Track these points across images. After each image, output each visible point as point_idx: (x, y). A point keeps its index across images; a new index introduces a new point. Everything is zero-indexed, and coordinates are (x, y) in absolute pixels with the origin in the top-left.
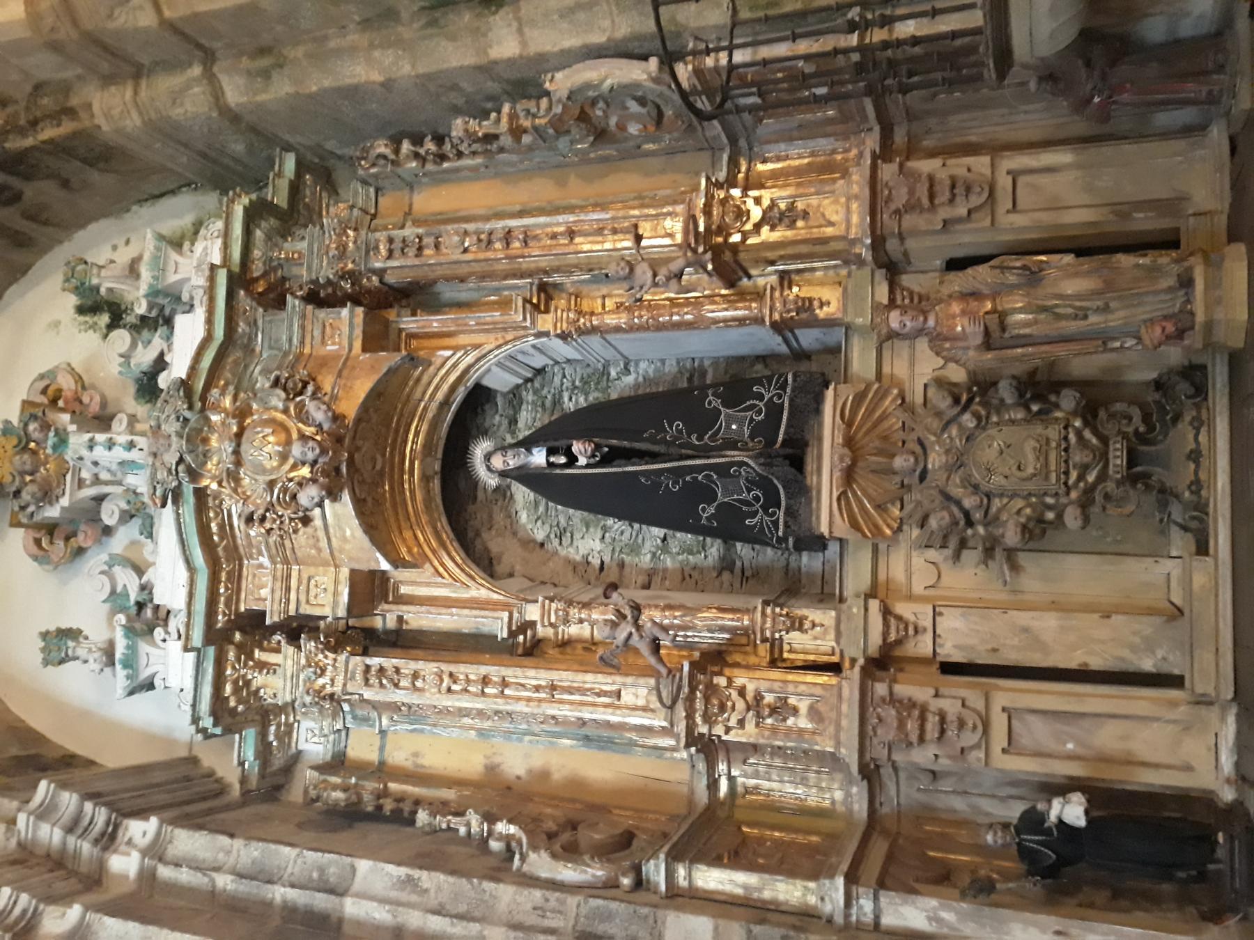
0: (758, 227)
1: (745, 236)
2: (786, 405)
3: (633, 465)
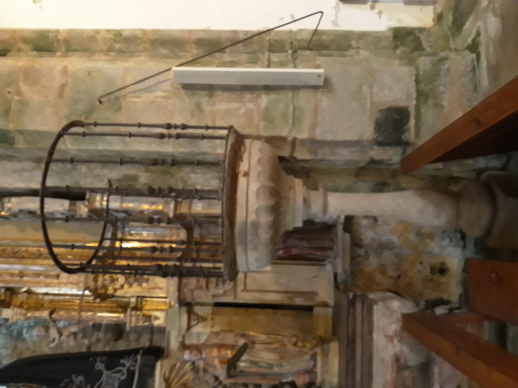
0: (122, 287)
1: (115, 290)
2: (137, 372)
3: (107, 317)
